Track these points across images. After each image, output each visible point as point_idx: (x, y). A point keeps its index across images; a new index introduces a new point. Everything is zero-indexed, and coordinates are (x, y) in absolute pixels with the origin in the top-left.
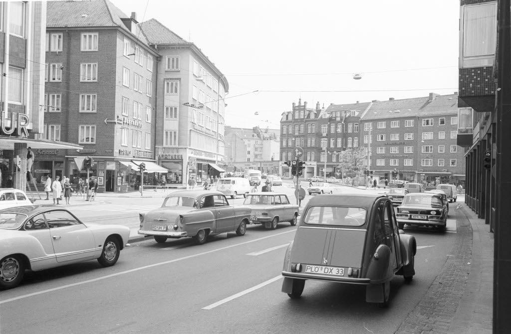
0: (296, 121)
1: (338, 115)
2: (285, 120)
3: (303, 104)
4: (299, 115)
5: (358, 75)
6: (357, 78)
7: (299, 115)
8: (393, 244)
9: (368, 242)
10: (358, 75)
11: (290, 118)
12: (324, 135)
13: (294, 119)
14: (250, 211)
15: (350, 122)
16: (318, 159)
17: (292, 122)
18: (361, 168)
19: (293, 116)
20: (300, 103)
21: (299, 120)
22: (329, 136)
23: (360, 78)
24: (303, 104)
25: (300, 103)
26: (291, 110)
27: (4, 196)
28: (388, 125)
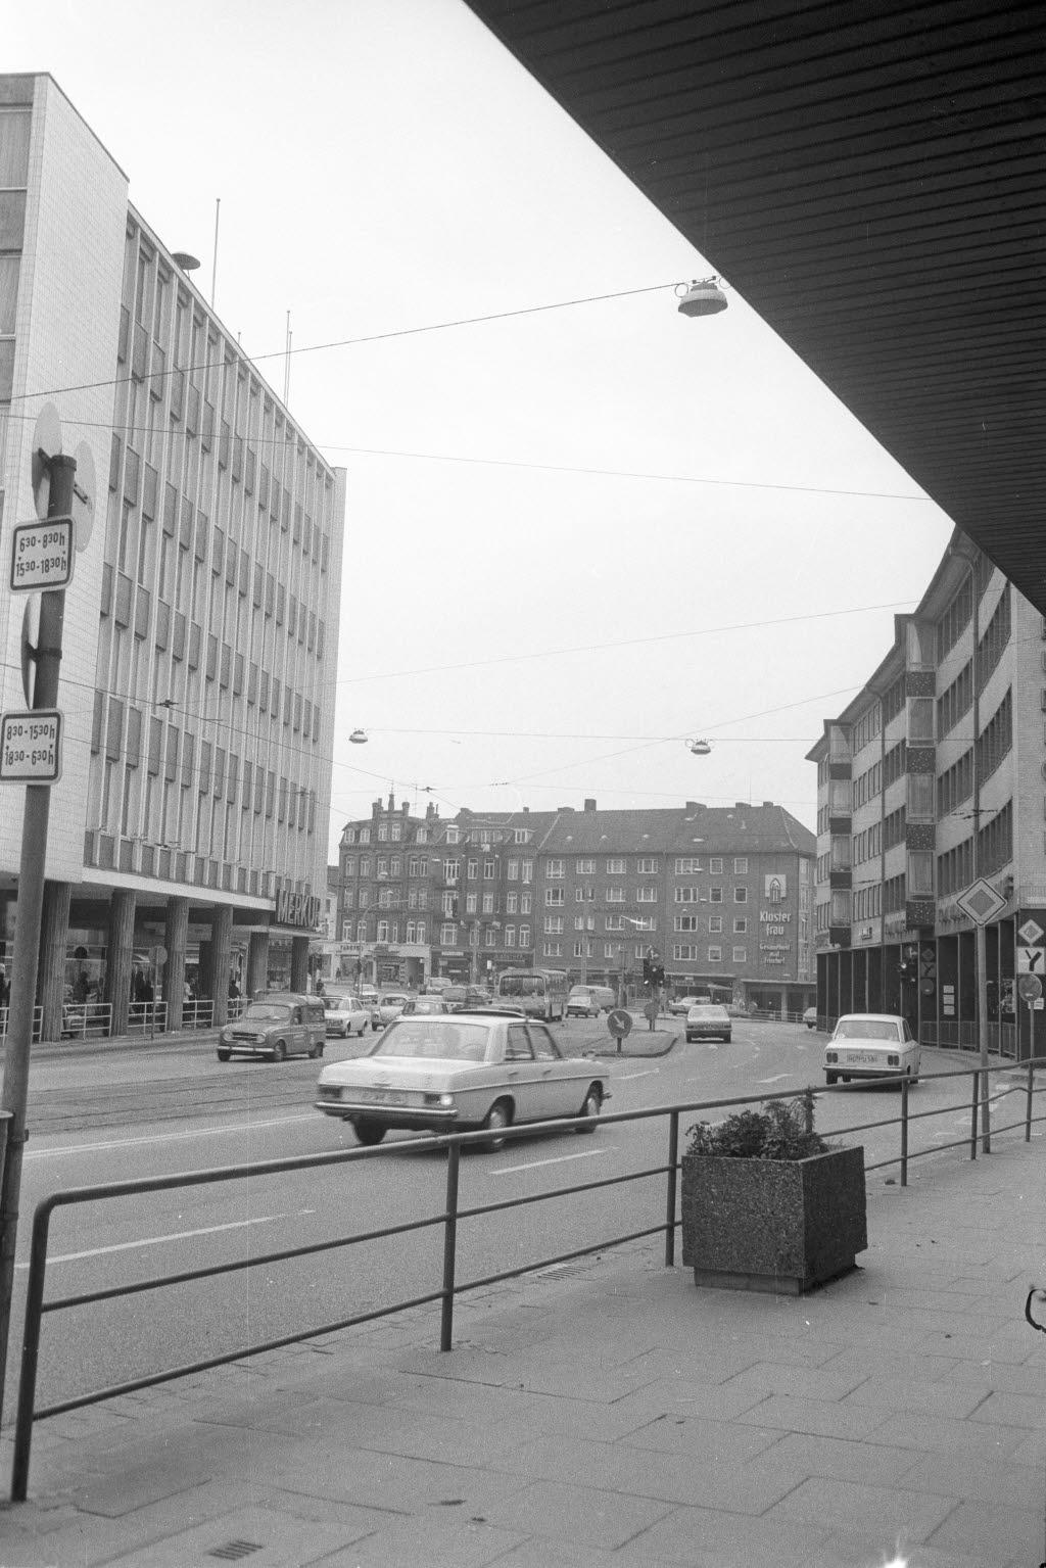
0: (379, 849)
1: (486, 836)
2: (351, 841)
3: (398, 807)
4: (390, 832)
5: (362, 733)
6: (701, 750)
7: (390, 832)
8: (140, 1043)
9: (428, 1118)
10: (362, 733)
11: (365, 839)
12: (451, 882)
13: (378, 842)
14: (429, 1077)
15: (512, 857)
16: (432, 940)
17: (369, 848)
18: (677, 983)
19: (374, 835)
20: (391, 803)
21: (388, 845)
22: (462, 886)
23: (707, 752)
24: (398, 807)
25: (391, 803)
26: (368, 815)
27: (42, 1040)
28: (601, 869)
